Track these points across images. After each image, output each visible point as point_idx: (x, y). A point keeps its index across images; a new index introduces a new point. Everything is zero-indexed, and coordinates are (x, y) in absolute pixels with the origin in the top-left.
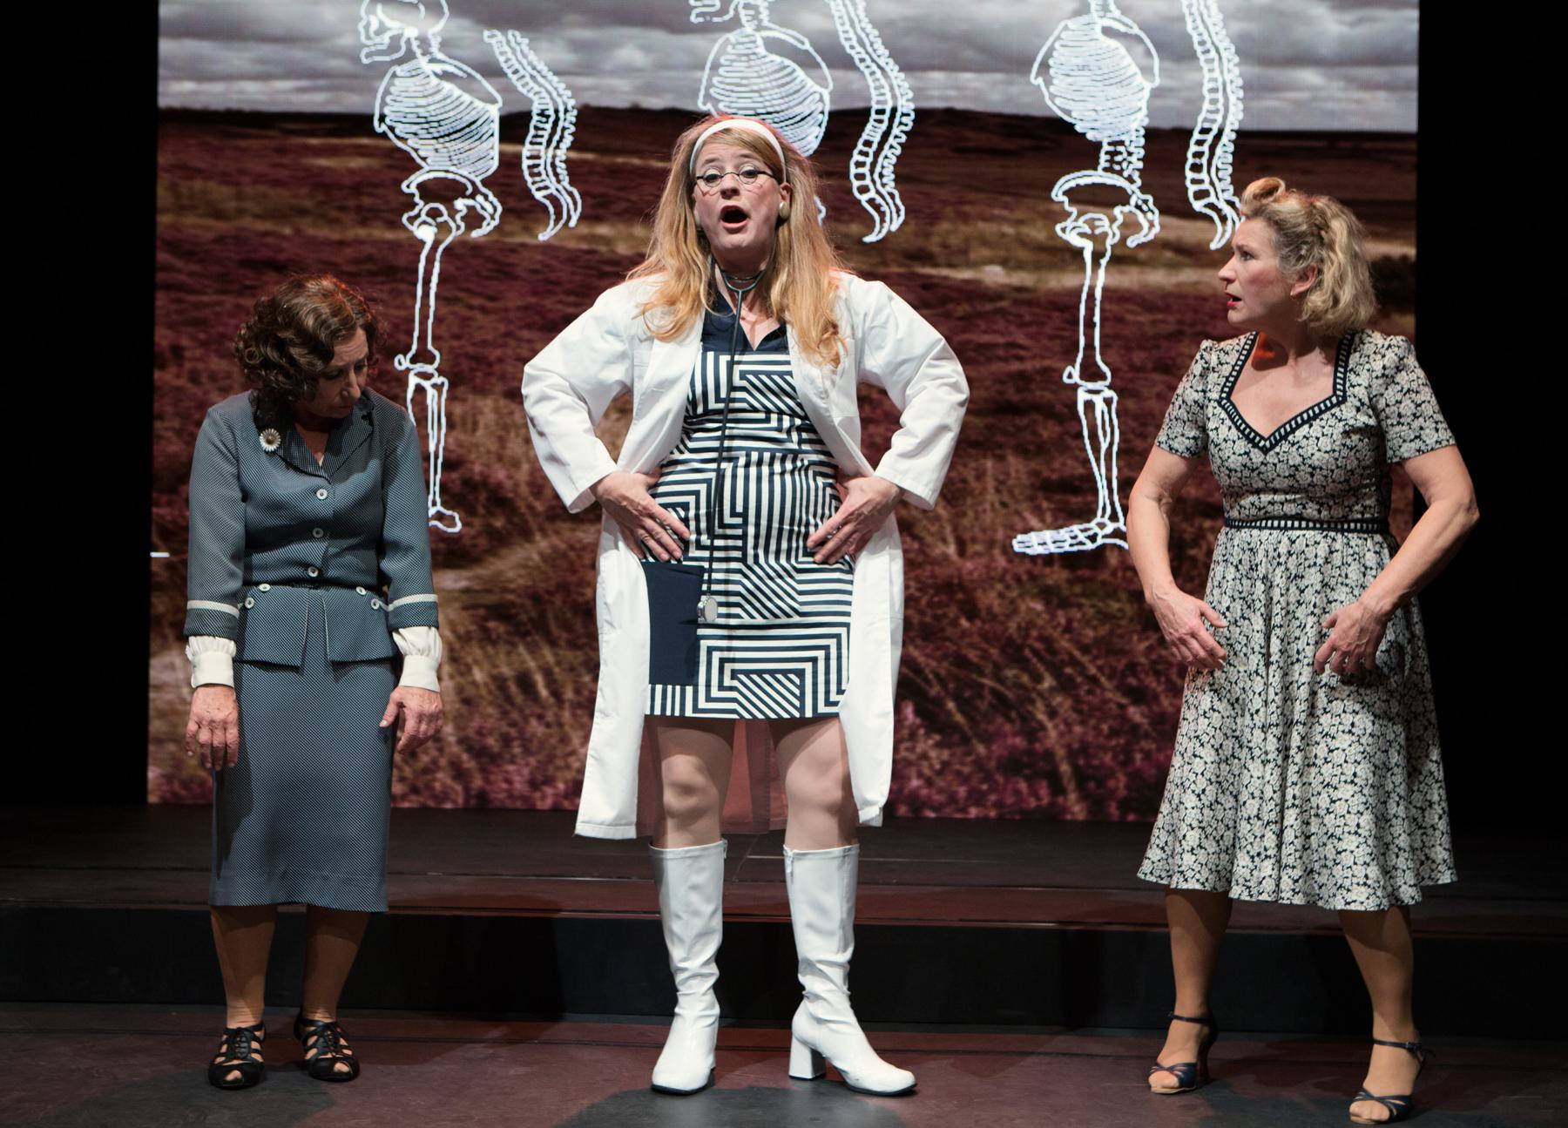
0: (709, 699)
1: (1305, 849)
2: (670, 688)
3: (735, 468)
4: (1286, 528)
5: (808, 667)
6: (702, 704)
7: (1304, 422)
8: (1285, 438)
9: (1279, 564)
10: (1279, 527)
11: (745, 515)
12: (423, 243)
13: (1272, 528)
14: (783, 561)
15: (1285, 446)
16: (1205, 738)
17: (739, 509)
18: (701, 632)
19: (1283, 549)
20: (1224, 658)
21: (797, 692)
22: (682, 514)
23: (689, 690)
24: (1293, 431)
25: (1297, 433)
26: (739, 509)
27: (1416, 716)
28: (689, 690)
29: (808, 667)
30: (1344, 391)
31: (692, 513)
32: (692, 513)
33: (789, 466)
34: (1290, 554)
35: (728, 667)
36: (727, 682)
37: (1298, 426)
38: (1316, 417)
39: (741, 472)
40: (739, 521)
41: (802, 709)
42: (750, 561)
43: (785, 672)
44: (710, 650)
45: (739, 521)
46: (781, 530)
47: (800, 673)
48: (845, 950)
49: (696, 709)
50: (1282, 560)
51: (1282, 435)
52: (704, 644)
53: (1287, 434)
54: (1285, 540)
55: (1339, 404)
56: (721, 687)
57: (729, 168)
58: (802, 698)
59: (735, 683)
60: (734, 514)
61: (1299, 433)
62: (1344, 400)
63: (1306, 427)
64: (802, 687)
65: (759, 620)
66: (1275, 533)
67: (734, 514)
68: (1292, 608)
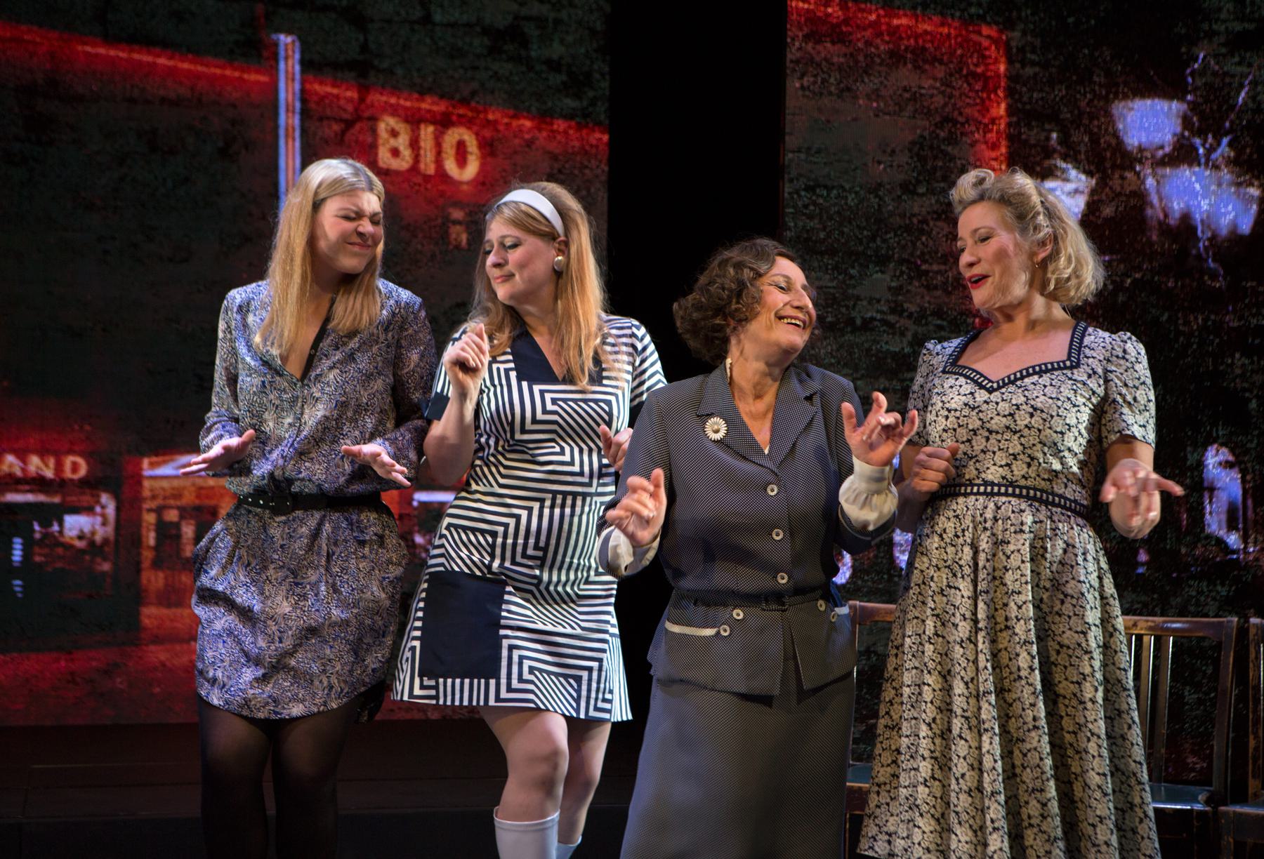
0: (510, 689)
2: (476, 681)
3: (542, 508)
4: (992, 494)
6: (504, 694)
7: (1035, 373)
9: (985, 529)
10: (985, 493)
11: (545, 549)
13: (978, 493)
14: (568, 589)
16: (924, 808)
17: (542, 544)
18: (502, 632)
19: (989, 514)
20: (846, 21)
21: (575, 695)
22: (490, 539)
23: (492, 682)
24: (1022, 378)
25: (1026, 380)
26: (542, 544)
28: (492, 682)
29: (585, 674)
30: (1078, 359)
31: (500, 540)
32: (500, 540)
34: (996, 519)
37: (1029, 375)
38: (1047, 371)
39: (547, 511)
40: (540, 554)
42: (542, 588)
45: (540, 554)
46: (563, 562)
47: (578, 679)
49: (498, 699)
50: (988, 525)
52: (505, 643)
53: (1016, 379)
54: (991, 505)
55: (1071, 368)
56: (521, 680)
58: (578, 701)
62: (1078, 365)
63: (1036, 377)
64: (579, 691)
66: (981, 499)
67: (536, 547)
68: (997, 574)
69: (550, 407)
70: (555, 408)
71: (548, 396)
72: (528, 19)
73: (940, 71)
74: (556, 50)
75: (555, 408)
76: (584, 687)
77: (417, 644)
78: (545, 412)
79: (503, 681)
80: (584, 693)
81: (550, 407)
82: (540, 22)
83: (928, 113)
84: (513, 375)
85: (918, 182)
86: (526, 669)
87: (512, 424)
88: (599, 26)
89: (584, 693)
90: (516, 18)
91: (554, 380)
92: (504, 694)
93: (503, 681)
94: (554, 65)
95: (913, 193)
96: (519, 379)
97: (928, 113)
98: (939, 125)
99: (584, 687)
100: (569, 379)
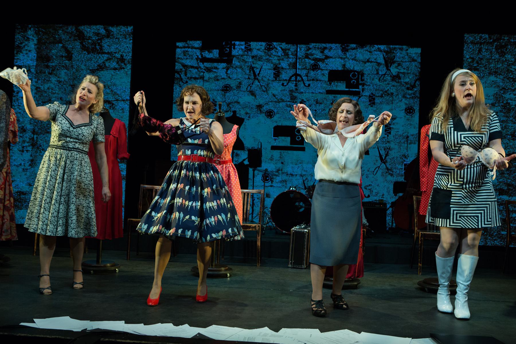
0: (453, 223)
1: (36, 193)
5: (480, 215)
8: (79, 127)
11: (463, 178)
12: (38, 105)
15: (79, 129)
17: (462, 177)
18: (451, 206)
23: (448, 220)
26: (462, 177)
27: (54, 171)
28: (448, 220)
33: (475, 165)
35: (458, 215)
36: (458, 218)
40: (462, 180)
41: (478, 226)
43: (473, 216)
44: (454, 210)
45: (462, 180)
47: (478, 217)
48: (467, 282)
51: (79, 126)
52: (452, 209)
56: (457, 220)
57: (367, 93)
58: (478, 223)
59: (460, 219)
60: (460, 178)
61: (82, 128)
64: (478, 220)
65: (467, 203)
67: (460, 178)
69: (463, 139)
70: (465, 140)
71: (462, 136)
72: (401, 73)
73: (502, 77)
74: (407, 80)
75: (465, 140)
76: (480, 219)
77: (429, 207)
78: (461, 141)
79: (451, 220)
80: (480, 220)
81: (463, 139)
82: (404, 73)
83: (498, 86)
84: (452, 129)
85: (495, 103)
86: (458, 216)
87: (451, 145)
88: (417, 74)
89: (480, 220)
90: (398, 73)
91: (465, 130)
92: (451, 224)
93: (451, 220)
94: (407, 83)
95: (494, 106)
96: (454, 130)
97: (498, 86)
98: (501, 90)
99: (480, 219)
100: (470, 129)
